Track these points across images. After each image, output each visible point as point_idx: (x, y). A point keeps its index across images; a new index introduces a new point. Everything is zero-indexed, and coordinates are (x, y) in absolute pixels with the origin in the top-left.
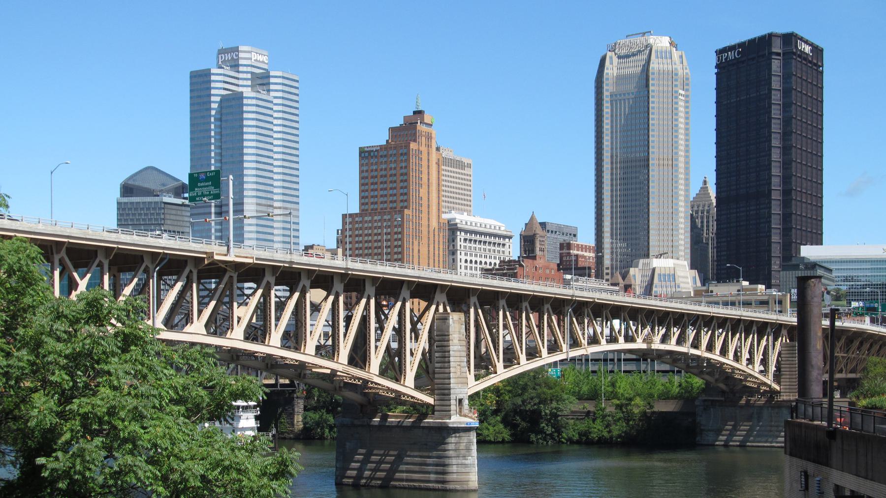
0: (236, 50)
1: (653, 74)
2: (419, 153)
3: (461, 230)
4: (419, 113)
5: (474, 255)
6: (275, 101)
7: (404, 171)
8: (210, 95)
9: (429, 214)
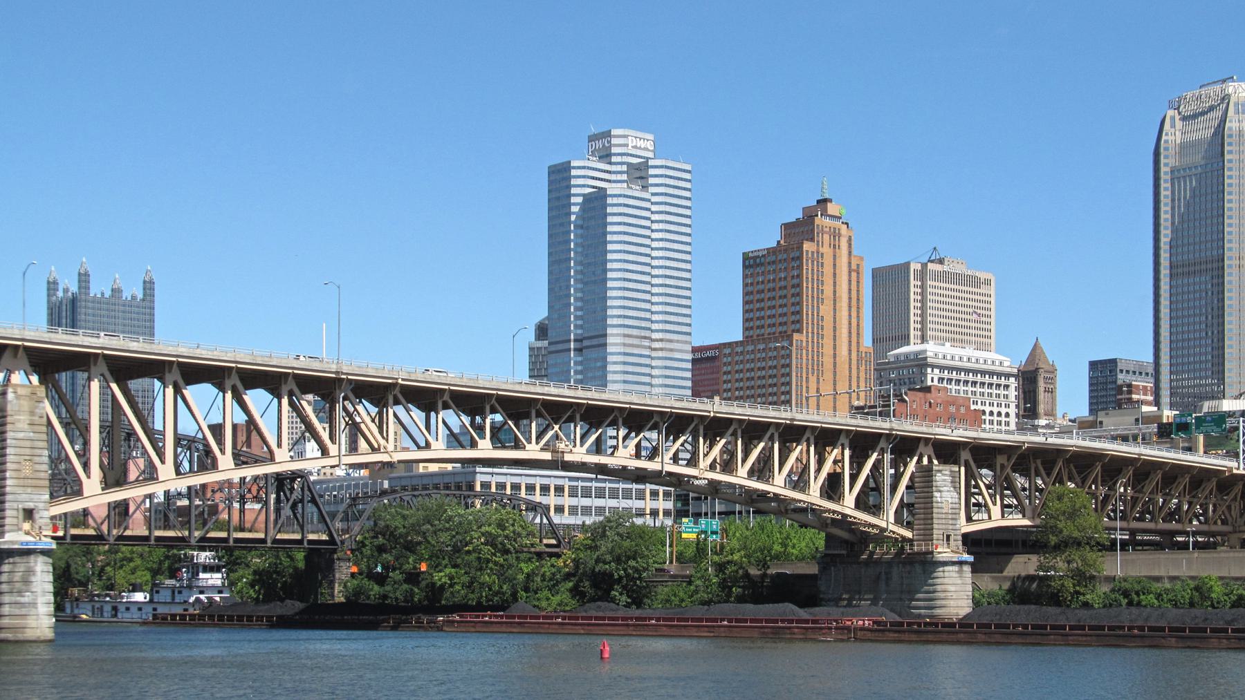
0: (607, 134)
1: (1230, 136)
2: (818, 256)
3: (933, 367)
4: (823, 202)
5: (1003, 405)
6: (654, 199)
7: (795, 281)
8: (569, 196)
9: (835, 340)
